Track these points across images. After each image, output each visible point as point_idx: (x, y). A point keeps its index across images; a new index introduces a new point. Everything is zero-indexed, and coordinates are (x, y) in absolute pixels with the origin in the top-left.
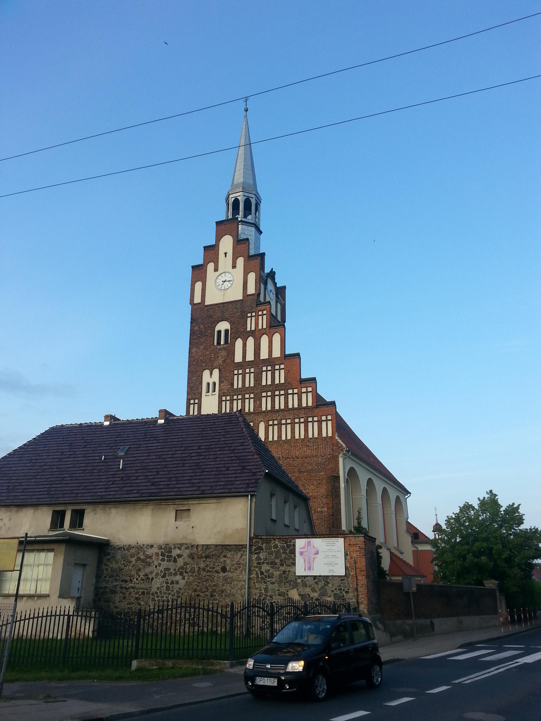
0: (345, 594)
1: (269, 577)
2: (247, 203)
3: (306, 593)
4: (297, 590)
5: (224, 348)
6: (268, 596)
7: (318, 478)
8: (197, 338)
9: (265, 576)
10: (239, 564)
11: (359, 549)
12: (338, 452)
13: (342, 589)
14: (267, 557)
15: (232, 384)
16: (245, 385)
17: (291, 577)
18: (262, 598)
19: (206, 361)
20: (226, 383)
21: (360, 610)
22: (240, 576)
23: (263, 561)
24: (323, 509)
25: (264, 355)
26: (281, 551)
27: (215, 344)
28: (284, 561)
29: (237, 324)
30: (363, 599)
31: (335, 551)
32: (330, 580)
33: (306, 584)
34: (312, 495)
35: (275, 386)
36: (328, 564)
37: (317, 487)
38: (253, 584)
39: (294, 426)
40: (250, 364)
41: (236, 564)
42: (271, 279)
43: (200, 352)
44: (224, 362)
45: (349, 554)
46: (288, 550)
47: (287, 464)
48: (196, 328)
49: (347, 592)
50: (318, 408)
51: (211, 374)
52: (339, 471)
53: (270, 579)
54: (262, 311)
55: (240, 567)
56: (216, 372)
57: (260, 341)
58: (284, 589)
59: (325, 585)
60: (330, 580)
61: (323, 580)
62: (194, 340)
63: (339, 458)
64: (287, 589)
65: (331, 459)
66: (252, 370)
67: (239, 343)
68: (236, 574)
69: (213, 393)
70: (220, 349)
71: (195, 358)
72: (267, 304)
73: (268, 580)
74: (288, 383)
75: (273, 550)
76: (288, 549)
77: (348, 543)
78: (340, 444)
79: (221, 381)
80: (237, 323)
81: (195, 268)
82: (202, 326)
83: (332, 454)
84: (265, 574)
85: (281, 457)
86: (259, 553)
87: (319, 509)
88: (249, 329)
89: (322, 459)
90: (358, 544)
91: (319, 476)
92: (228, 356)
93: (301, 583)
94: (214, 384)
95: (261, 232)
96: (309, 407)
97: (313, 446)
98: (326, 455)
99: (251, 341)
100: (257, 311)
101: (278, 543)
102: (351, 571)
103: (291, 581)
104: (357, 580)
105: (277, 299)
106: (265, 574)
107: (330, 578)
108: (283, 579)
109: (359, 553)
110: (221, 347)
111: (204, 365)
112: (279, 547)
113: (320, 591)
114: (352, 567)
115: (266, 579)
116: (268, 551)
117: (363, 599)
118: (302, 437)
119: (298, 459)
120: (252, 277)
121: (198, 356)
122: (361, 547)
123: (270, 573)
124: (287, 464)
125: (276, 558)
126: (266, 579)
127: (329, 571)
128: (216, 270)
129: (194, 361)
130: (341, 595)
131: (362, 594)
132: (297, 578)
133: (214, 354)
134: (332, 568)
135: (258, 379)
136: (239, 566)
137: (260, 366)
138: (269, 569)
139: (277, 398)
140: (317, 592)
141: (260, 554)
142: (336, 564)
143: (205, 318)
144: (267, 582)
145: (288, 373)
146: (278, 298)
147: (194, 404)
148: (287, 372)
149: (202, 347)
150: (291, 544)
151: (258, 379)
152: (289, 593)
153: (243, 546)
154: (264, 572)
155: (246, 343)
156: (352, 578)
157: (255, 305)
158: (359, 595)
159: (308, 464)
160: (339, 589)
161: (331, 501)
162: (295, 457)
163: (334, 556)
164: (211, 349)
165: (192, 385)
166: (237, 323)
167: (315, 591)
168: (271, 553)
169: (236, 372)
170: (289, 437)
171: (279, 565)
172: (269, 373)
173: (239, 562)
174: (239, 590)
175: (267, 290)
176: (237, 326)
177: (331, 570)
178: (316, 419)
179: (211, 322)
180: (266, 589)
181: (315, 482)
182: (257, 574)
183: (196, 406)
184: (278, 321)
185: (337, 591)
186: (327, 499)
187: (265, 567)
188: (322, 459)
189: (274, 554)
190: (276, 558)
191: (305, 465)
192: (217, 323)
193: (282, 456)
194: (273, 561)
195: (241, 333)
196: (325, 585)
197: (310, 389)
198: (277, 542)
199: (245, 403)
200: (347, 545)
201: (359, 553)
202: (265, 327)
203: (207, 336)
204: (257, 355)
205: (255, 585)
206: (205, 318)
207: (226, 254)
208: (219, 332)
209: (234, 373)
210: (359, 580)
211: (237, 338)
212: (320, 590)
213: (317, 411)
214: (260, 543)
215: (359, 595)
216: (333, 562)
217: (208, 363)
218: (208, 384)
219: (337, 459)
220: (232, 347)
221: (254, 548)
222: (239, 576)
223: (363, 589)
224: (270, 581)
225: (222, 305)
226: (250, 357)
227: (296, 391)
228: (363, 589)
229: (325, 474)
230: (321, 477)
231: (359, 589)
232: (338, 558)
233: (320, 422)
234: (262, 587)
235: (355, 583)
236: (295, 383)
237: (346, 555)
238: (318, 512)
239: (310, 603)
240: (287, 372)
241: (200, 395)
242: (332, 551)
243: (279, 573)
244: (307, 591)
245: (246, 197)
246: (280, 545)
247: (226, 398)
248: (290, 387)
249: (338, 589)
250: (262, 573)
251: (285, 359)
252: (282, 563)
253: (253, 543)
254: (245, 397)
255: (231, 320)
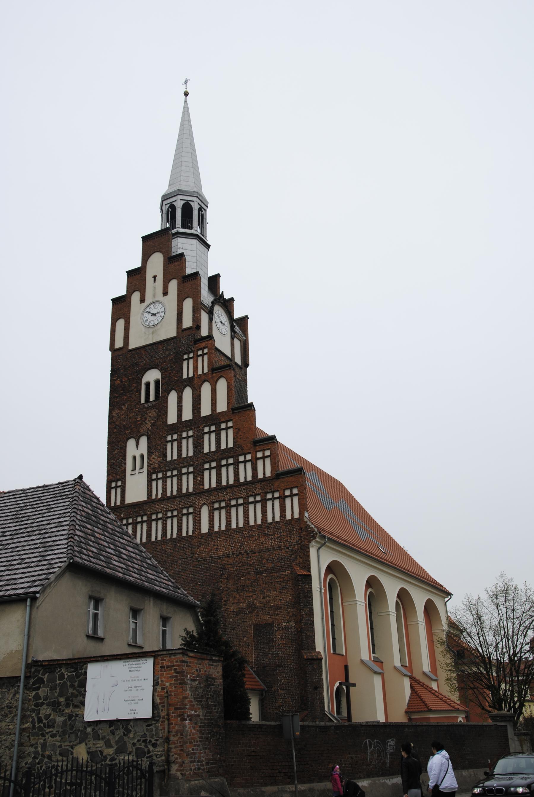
0: (151, 748)
1: (49, 727)
2: (187, 208)
3: (98, 749)
4: (86, 744)
5: (154, 406)
6: (46, 756)
7: (282, 580)
8: (118, 397)
9: (44, 724)
10: (11, 707)
11: (175, 674)
12: (308, 539)
13: (148, 741)
14: (49, 695)
15: (165, 455)
16: (181, 455)
17: (79, 725)
18: (37, 761)
19: (131, 426)
20: (156, 454)
21: (171, 774)
22: (10, 727)
23: (42, 701)
24: (290, 624)
25: (206, 410)
26: (68, 683)
27: (143, 401)
28: (71, 699)
29: (169, 372)
30: (176, 756)
31: (141, 680)
32: (131, 726)
33: (99, 735)
34: (274, 605)
35: (221, 453)
36: (130, 700)
37: (281, 593)
38: (26, 738)
39: (248, 508)
40: (188, 425)
41: (6, 708)
42: (221, 307)
43: (123, 415)
44: (153, 425)
45: (160, 683)
46: (77, 682)
47: (239, 563)
48: (118, 382)
49: (155, 745)
50: (279, 478)
51: (137, 444)
52: (310, 568)
53: (51, 730)
54: (202, 349)
55: (11, 713)
56: (144, 441)
57: (200, 392)
58: (68, 744)
59: (125, 735)
60: (131, 726)
61: (121, 726)
62: (115, 399)
63: (309, 548)
64: (72, 744)
65: (298, 551)
66: (191, 433)
67: (173, 397)
68: (6, 724)
69: (141, 471)
70: (149, 408)
71: (117, 423)
72: (209, 339)
73: (48, 730)
74: (239, 447)
75: (58, 682)
76: (77, 680)
77: (160, 665)
78: (311, 528)
79: (150, 453)
80: (170, 370)
81: (116, 301)
82: (125, 379)
83: (300, 544)
84: (44, 722)
85: (231, 553)
86: (38, 688)
87: (284, 624)
88: (185, 376)
89: (287, 552)
90: (173, 666)
91: (282, 576)
92: (159, 416)
93: (91, 733)
94: (142, 456)
95: (208, 246)
96: (267, 479)
97: (274, 534)
98: (291, 545)
99: (188, 393)
100: (195, 350)
101: (65, 672)
102: (162, 710)
103: (79, 730)
104: (169, 724)
105: (233, 334)
106: (44, 722)
107: (132, 723)
108: (68, 729)
109: (175, 681)
110: (150, 404)
111: (128, 432)
112: (66, 676)
113: (116, 745)
114: (163, 703)
115: (45, 729)
116: (50, 684)
117: (176, 756)
118: (259, 522)
119: (253, 555)
120: (188, 304)
121: (120, 421)
122: (178, 670)
123: (51, 720)
124: (239, 563)
125: (61, 695)
126: (45, 729)
127: (130, 712)
128: (142, 300)
129: (115, 428)
130: (146, 750)
131: (175, 747)
132: (86, 726)
133: (140, 416)
134: (133, 707)
135: (198, 445)
136: (10, 711)
137: (201, 427)
138: (49, 713)
139: (224, 470)
140: (113, 747)
141: (39, 690)
142: (140, 700)
143: (129, 367)
144: (46, 735)
145: (238, 433)
146: (235, 332)
147: (116, 487)
148: (236, 431)
149: (125, 408)
150: (82, 672)
151: (198, 445)
152: (74, 751)
153: (18, 678)
154: (43, 719)
155: (182, 396)
156: (162, 722)
157: (193, 342)
158: (171, 748)
159: (267, 560)
160: (144, 741)
161: (299, 611)
162: (250, 552)
163: (138, 687)
164: (137, 409)
165: (112, 461)
166: (170, 370)
167: (111, 746)
168: (53, 688)
169: (169, 438)
170: (241, 525)
171: (64, 706)
172: (213, 436)
173: (10, 705)
174: (7, 749)
175: (213, 321)
176: (170, 373)
177: (133, 710)
178: (277, 495)
179: (136, 372)
180: (44, 746)
181: (278, 586)
182: (33, 722)
183: (119, 490)
184: (236, 364)
185: (140, 744)
186: (294, 609)
187: (45, 710)
188: (287, 552)
189: (58, 689)
190: (61, 695)
191: (264, 562)
192: (145, 373)
193: (233, 552)
194: (56, 700)
195: (175, 383)
196: (125, 735)
197: (267, 453)
198: (63, 671)
199: (181, 480)
200: (158, 668)
201: (175, 681)
202: (206, 371)
203: (131, 392)
204: (196, 411)
205: (30, 739)
206: (129, 367)
207: (155, 277)
208: (148, 385)
209: (166, 439)
210: (172, 724)
211: (170, 391)
212: (117, 742)
213: (277, 483)
214: (41, 672)
215: (171, 748)
216: (136, 697)
217: (134, 429)
218: (135, 458)
219: (307, 550)
220: (164, 403)
221: (32, 680)
222: (9, 726)
223: (176, 738)
224: (50, 732)
225: (150, 347)
226: (187, 415)
227: (249, 457)
228: (176, 738)
229: (291, 573)
230: (286, 578)
231: (172, 738)
232: (143, 689)
233: (282, 499)
234: (39, 743)
235: (166, 729)
236: (247, 446)
237: (156, 683)
238: (283, 629)
239: (102, 765)
240: (236, 431)
241: (123, 474)
242: (136, 679)
243: (62, 719)
244: (98, 745)
245: (184, 202)
246: (67, 675)
247: (157, 476)
248: (241, 452)
249: (142, 740)
250: (40, 720)
251: (233, 413)
252: (68, 702)
253: (30, 673)
254: (181, 472)
255: (162, 367)
